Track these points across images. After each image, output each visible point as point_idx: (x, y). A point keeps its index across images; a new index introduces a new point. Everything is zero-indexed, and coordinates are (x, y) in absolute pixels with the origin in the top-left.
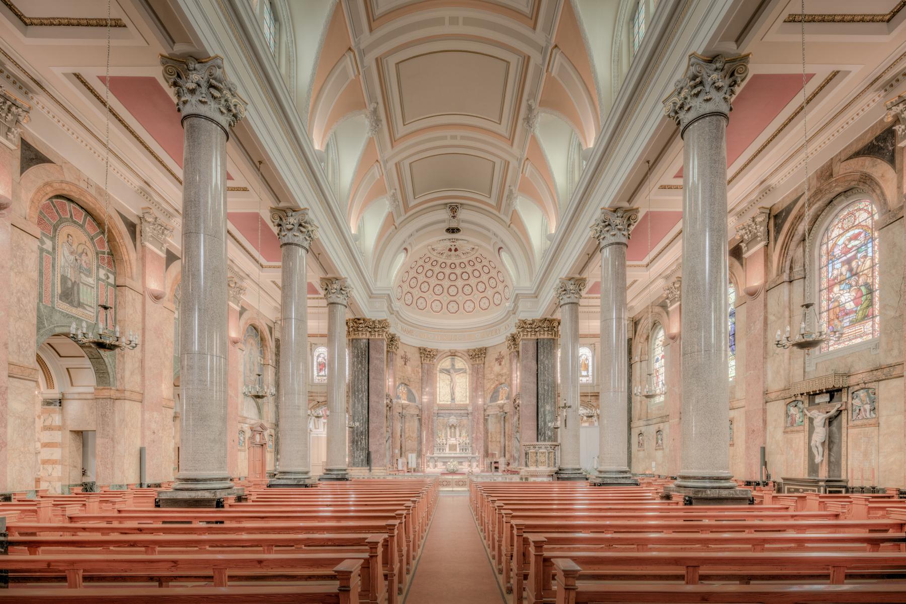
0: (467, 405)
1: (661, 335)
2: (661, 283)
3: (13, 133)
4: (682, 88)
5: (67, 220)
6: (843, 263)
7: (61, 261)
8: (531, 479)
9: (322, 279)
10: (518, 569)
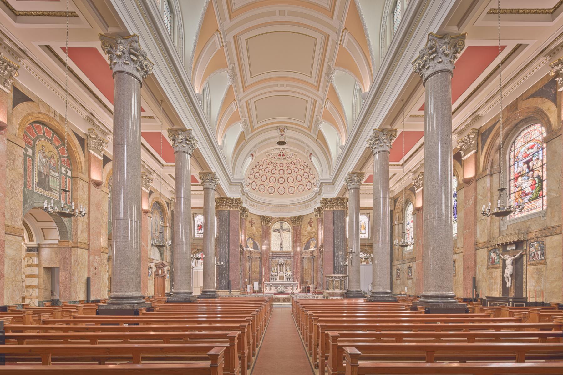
0: (290, 252)
1: (411, 208)
2: (411, 175)
3: (8, 83)
4: (424, 55)
5: (41, 137)
6: (525, 163)
7: (38, 162)
8: (331, 298)
10: (322, 353)
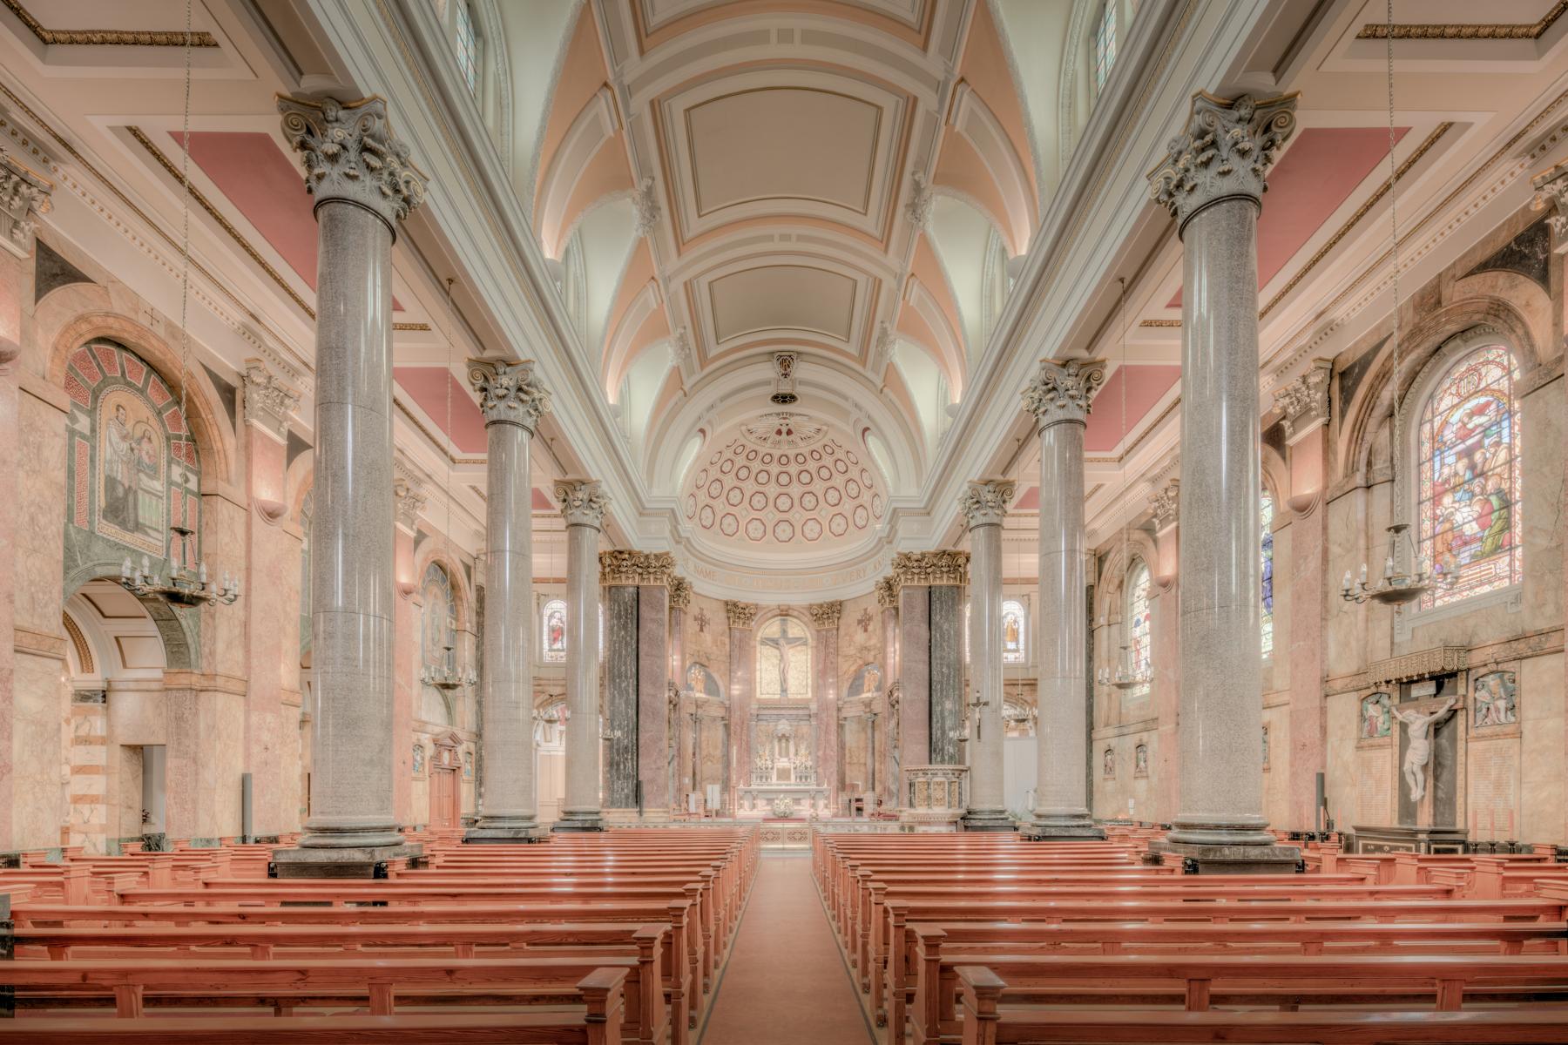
0: (808, 701)
1: (1144, 580)
2: (1144, 489)
3: (22, 230)
4: (1180, 153)
5: (116, 381)
6: (1460, 456)
7: (105, 452)
8: (920, 829)
9: (558, 483)
10: (897, 984)
